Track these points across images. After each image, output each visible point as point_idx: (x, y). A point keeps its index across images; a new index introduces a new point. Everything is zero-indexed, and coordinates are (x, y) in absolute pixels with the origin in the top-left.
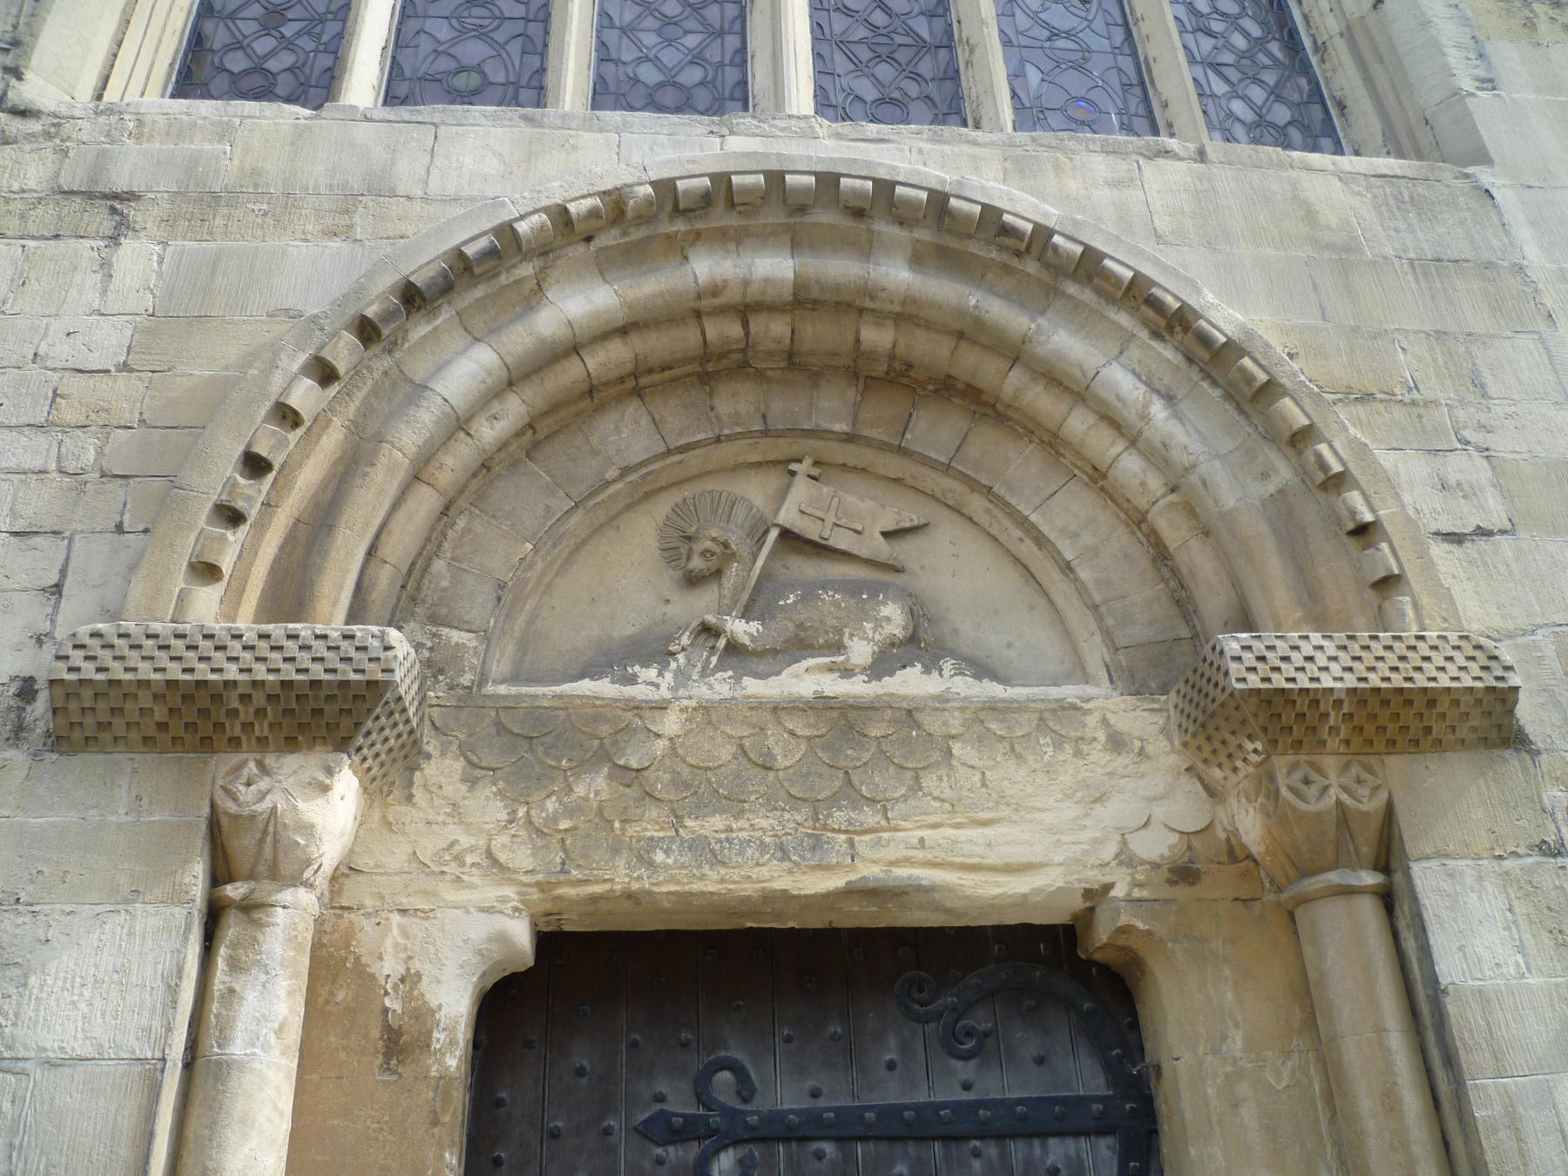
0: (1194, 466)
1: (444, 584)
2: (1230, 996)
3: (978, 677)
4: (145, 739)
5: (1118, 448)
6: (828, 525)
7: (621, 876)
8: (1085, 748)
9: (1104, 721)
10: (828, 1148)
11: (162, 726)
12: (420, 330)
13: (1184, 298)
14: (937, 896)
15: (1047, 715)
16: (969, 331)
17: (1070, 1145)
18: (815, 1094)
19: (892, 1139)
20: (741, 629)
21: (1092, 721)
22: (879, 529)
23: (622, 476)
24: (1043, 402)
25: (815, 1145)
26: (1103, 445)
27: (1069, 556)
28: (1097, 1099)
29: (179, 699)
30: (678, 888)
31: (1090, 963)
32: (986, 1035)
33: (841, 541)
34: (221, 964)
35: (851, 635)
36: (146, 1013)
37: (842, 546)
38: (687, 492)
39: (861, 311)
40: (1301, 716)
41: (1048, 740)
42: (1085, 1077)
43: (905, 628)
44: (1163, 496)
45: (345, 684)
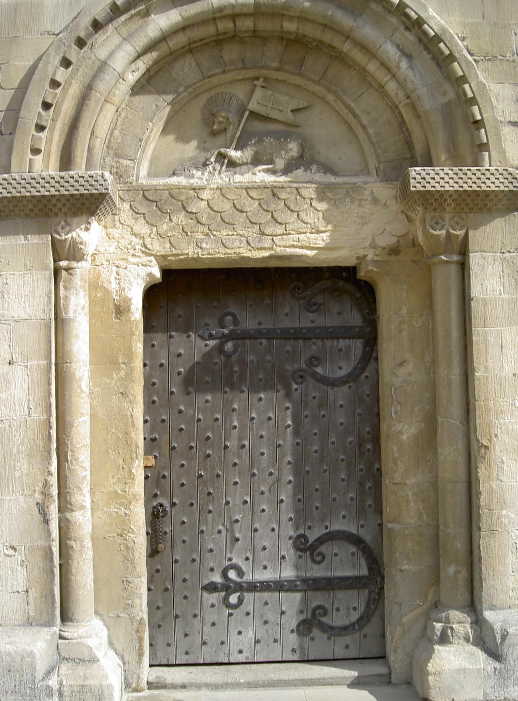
0: (415, 90)
1: (119, 140)
2: (404, 295)
3: (325, 173)
4: (26, 215)
5: (386, 79)
6: (269, 108)
7: (191, 251)
8: (363, 203)
9: (372, 193)
10: (264, 341)
11: (32, 210)
12: (100, 37)
13: (419, 13)
14: (303, 258)
15: (350, 190)
16: (327, 26)
17: (347, 341)
18: (260, 324)
19: (285, 339)
20: (234, 154)
21: (367, 192)
22: (290, 109)
23: (185, 90)
24: (357, 55)
25: (259, 340)
26: (382, 77)
27: (365, 122)
28: (358, 327)
29: (36, 201)
30: (211, 256)
31: (360, 281)
32: (321, 305)
33: (275, 115)
34: (62, 288)
35: (276, 157)
36: (42, 305)
37: (275, 117)
38: (213, 92)
39: (283, 15)
40: (436, 200)
41: (349, 200)
42: (354, 319)
43: (298, 152)
44: (404, 100)
45: (92, 195)
